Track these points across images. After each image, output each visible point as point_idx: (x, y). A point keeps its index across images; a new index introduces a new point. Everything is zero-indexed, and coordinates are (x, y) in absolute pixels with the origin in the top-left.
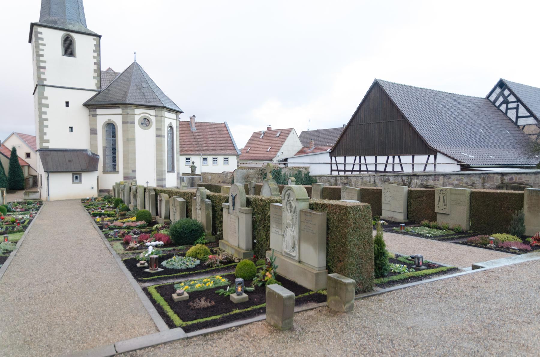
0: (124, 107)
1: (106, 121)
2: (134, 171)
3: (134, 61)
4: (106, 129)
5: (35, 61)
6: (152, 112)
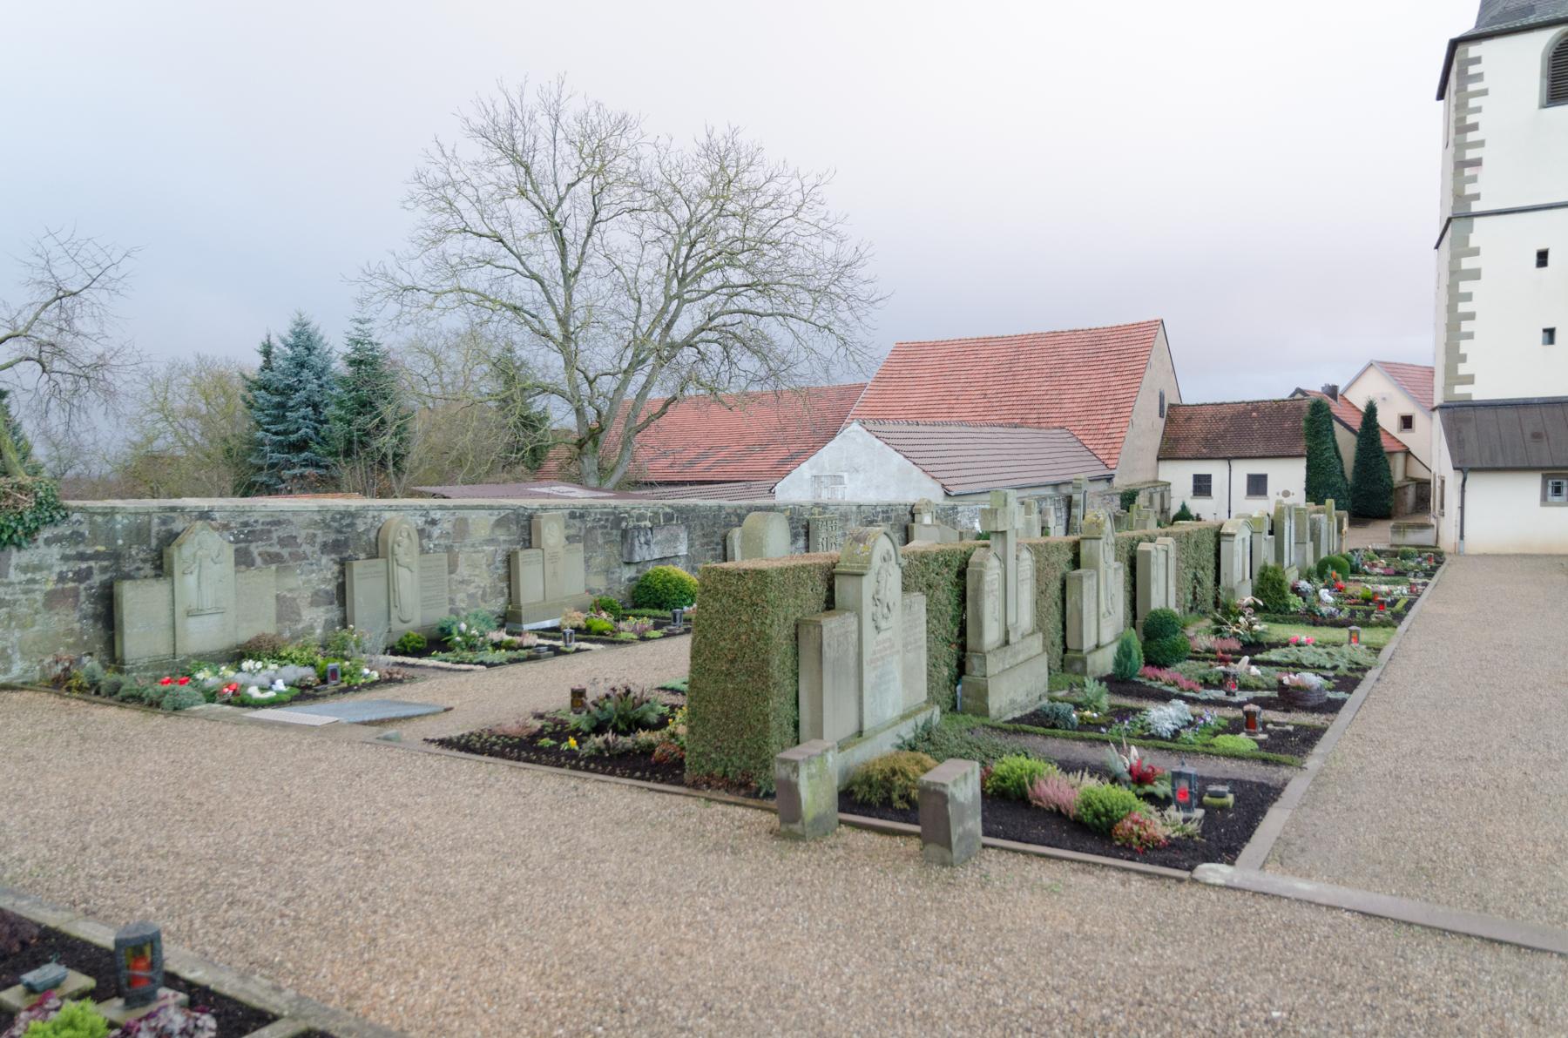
5: (1451, 148)
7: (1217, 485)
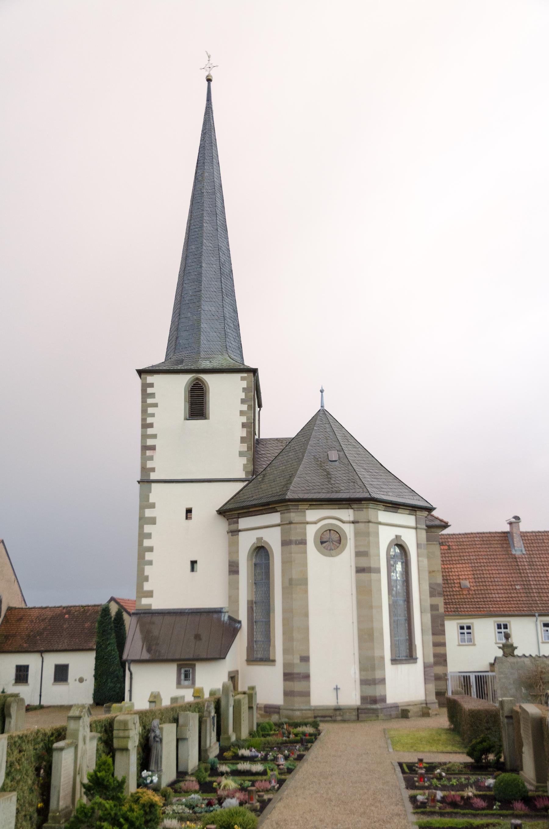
0: (284, 508)
1: (254, 543)
2: (305, 659)
3: (319, 408)
4: (254, 560)
6: (347, 514)
7: (33, 674)
